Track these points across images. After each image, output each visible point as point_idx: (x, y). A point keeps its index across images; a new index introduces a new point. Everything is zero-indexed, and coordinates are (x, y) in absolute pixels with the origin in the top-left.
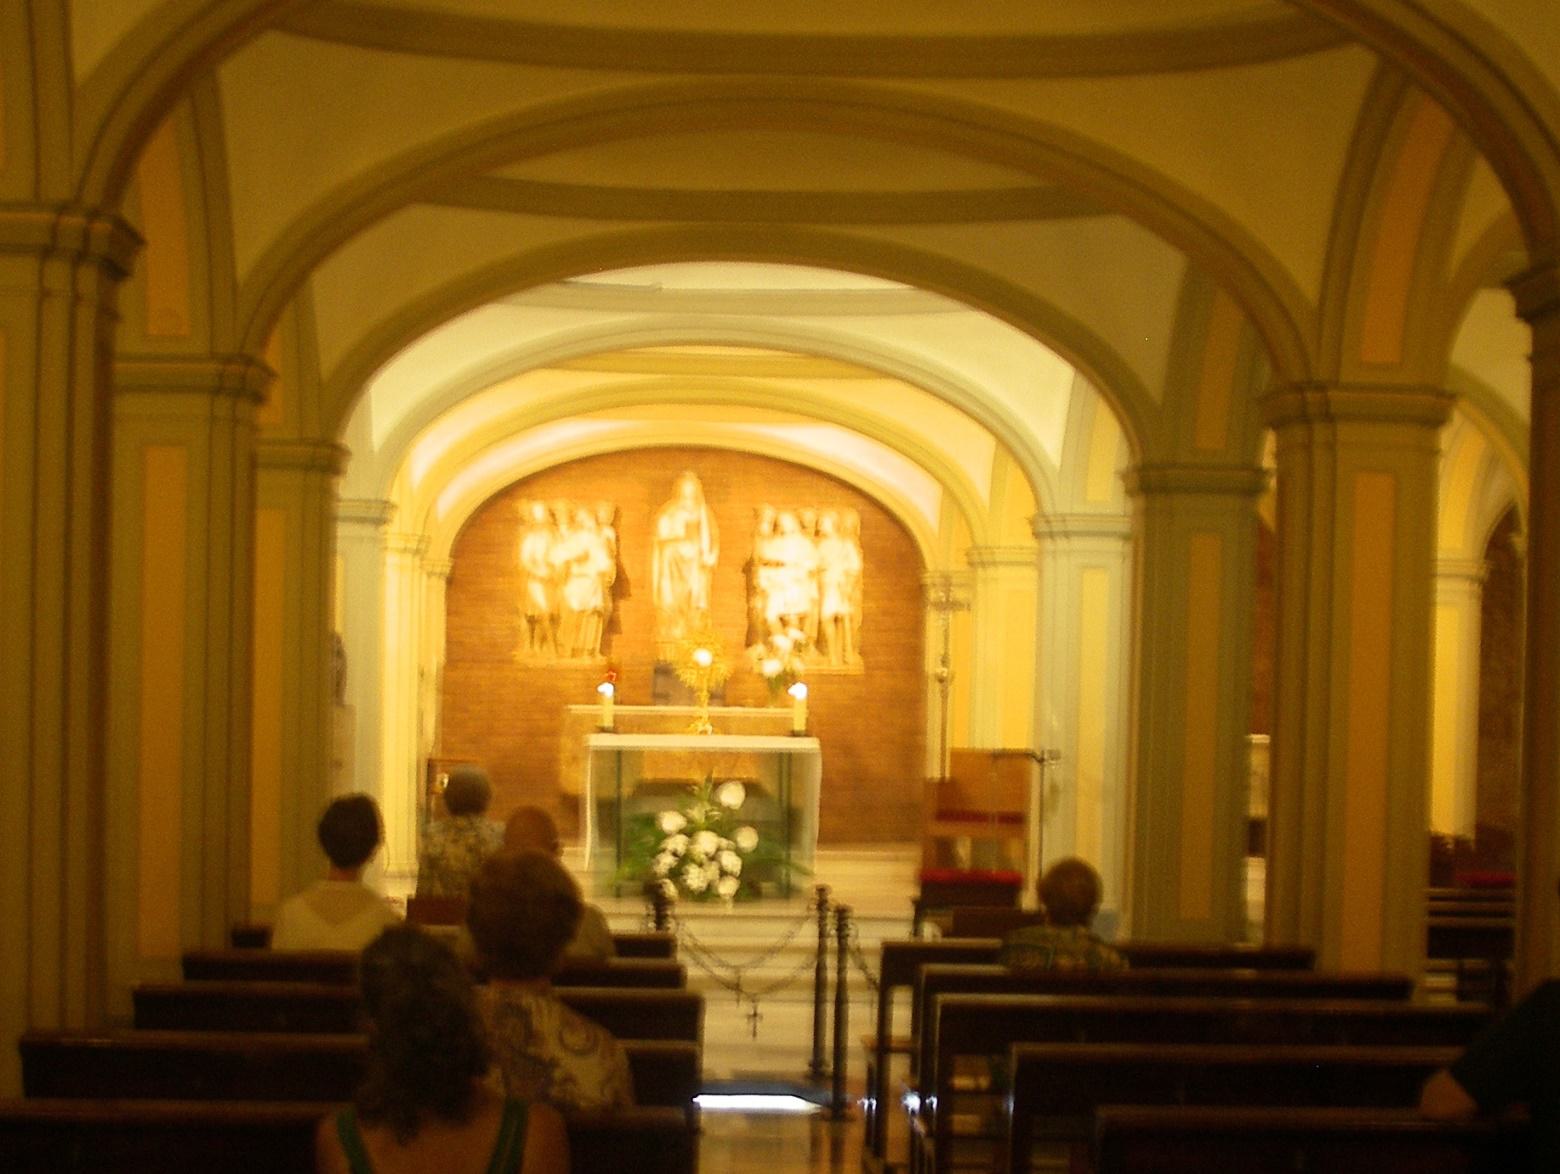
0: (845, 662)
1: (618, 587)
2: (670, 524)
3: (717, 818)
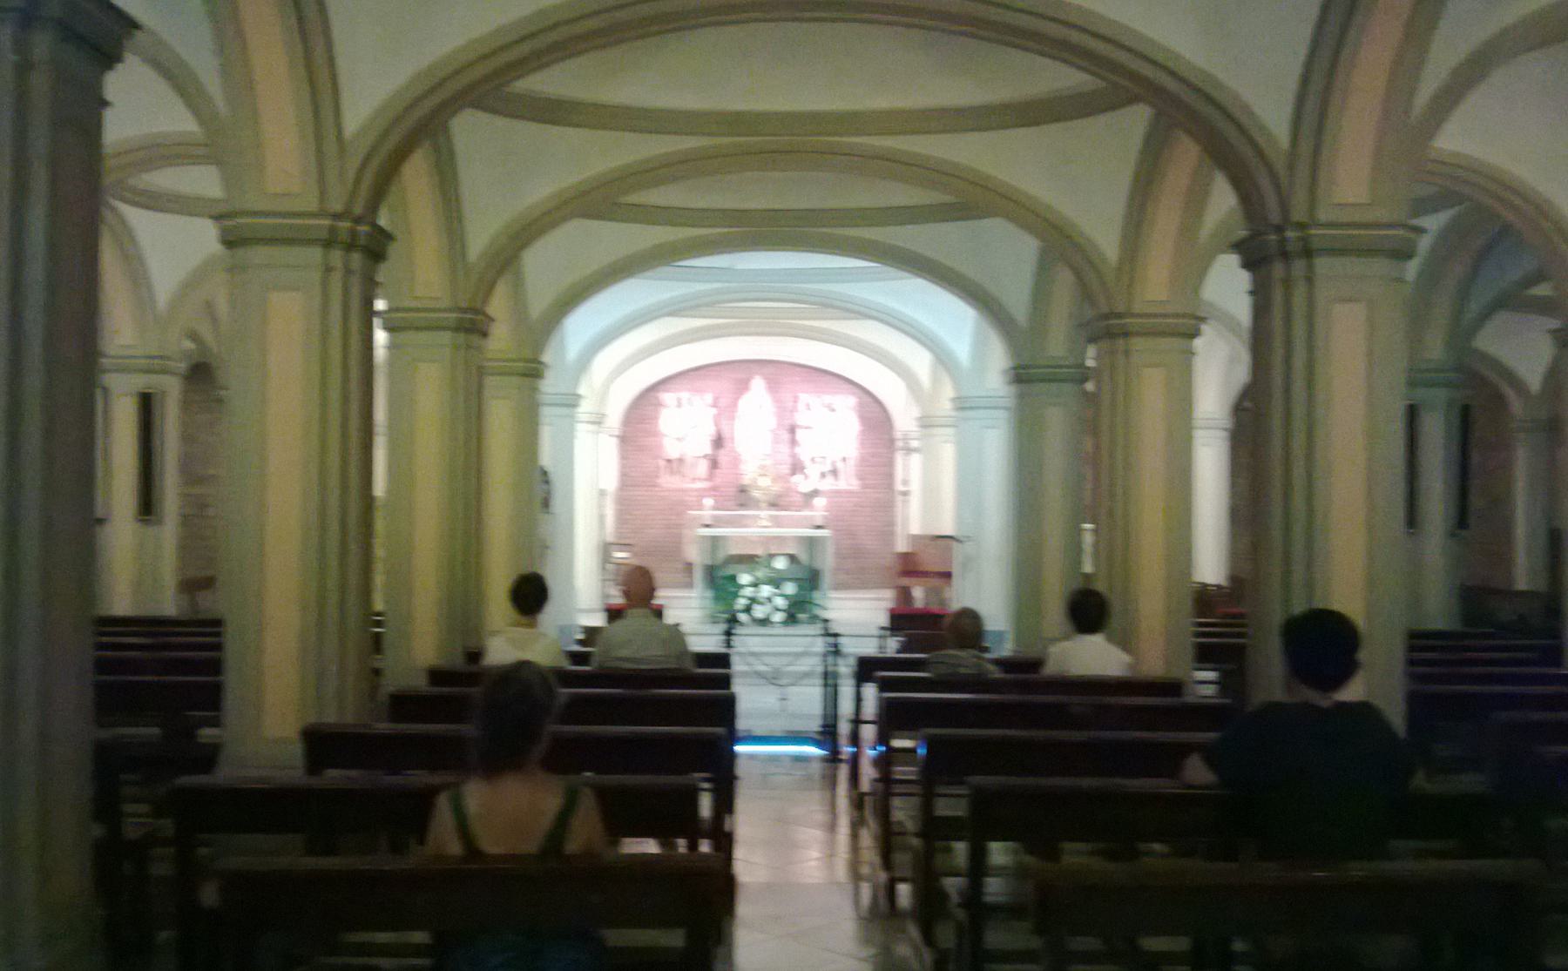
1: (718, 442)
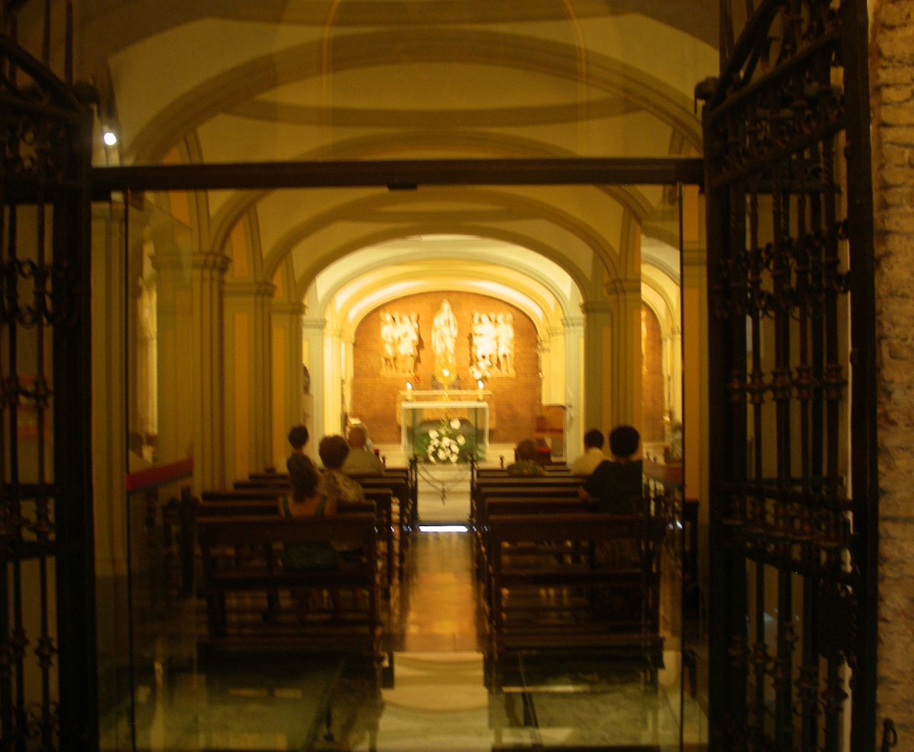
1: (420, 345)
2: (439, 321)
3: (450, 433)
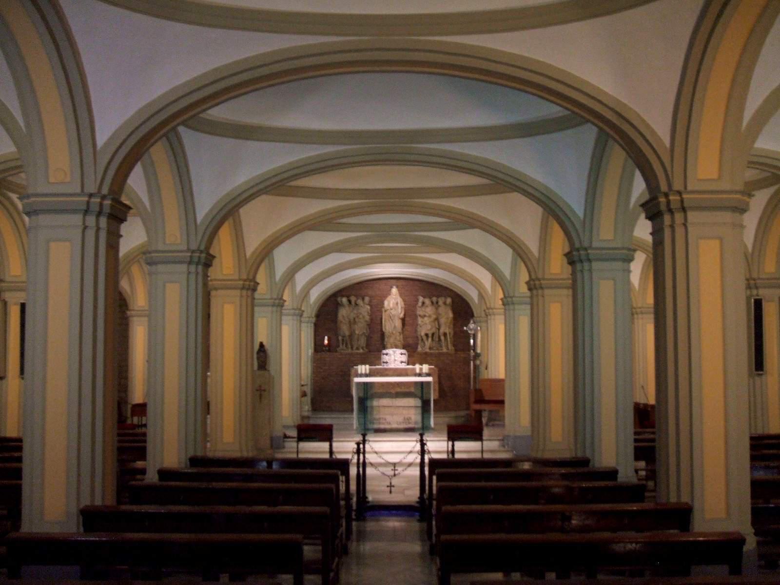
0: (448, 349)
